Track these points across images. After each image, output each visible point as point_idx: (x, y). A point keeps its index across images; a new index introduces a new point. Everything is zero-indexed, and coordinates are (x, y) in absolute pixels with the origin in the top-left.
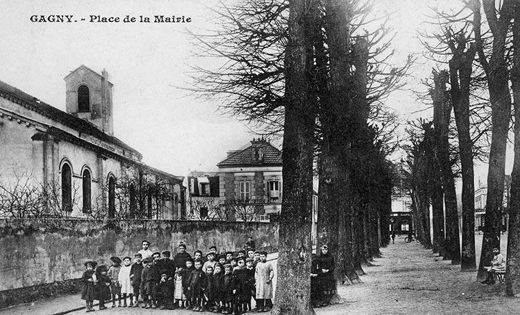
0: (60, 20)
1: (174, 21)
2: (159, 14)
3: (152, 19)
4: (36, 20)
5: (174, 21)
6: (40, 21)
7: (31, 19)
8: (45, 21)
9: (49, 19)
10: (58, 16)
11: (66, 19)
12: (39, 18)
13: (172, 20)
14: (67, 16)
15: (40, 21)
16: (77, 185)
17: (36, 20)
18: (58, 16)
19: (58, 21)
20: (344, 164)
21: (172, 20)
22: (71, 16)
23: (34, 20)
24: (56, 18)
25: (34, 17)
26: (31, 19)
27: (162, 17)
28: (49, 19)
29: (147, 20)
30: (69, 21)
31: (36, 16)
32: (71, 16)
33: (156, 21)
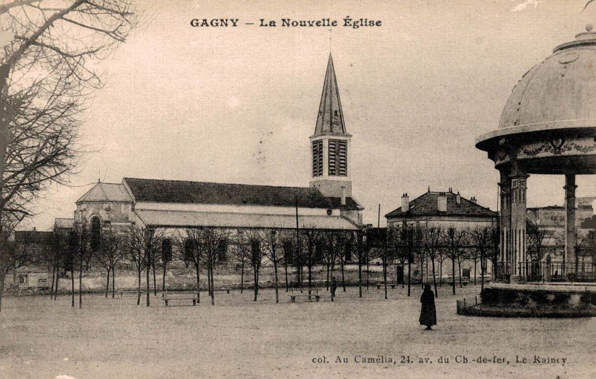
0: (285, 24)
1: (366, 25)
2: (286, 18)
3: (279, 23)
4: (197, 24)
5: (366, 25)
6: (202, 25)
7: (192, 23)
8: (207, 25)
9: (211, 23)
10: (222, 20)
11: (230, 23)
12: (201, 22)
13: (547, 361)
14: (232, 20)
15: (202, 25)
16: (514, 272)
17: (197, 24)
18: (222, 20)
19: (222, 25)
20: (462, 101)
21: (547, 361)
22: (237, 20)
23: (215, 25)
24: (307, 24)
25: (195, 22)
26: (192, 23)
27: (289, 20)
28: (211, 23)
29: (272, 24)
30: (235, 25)
31: (197, 20)
32: (237, 20)
33: (283, 25)
